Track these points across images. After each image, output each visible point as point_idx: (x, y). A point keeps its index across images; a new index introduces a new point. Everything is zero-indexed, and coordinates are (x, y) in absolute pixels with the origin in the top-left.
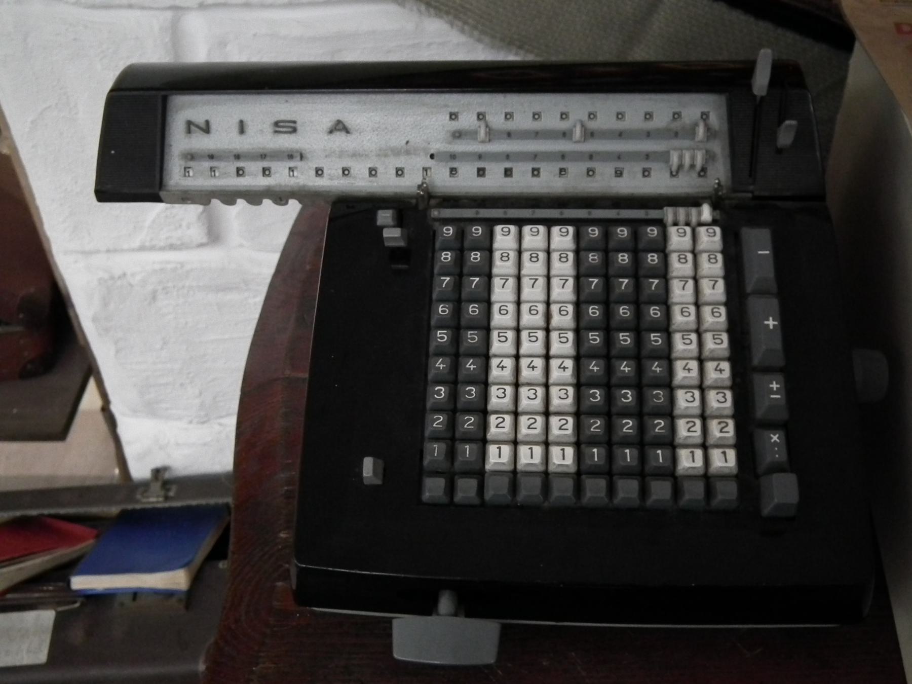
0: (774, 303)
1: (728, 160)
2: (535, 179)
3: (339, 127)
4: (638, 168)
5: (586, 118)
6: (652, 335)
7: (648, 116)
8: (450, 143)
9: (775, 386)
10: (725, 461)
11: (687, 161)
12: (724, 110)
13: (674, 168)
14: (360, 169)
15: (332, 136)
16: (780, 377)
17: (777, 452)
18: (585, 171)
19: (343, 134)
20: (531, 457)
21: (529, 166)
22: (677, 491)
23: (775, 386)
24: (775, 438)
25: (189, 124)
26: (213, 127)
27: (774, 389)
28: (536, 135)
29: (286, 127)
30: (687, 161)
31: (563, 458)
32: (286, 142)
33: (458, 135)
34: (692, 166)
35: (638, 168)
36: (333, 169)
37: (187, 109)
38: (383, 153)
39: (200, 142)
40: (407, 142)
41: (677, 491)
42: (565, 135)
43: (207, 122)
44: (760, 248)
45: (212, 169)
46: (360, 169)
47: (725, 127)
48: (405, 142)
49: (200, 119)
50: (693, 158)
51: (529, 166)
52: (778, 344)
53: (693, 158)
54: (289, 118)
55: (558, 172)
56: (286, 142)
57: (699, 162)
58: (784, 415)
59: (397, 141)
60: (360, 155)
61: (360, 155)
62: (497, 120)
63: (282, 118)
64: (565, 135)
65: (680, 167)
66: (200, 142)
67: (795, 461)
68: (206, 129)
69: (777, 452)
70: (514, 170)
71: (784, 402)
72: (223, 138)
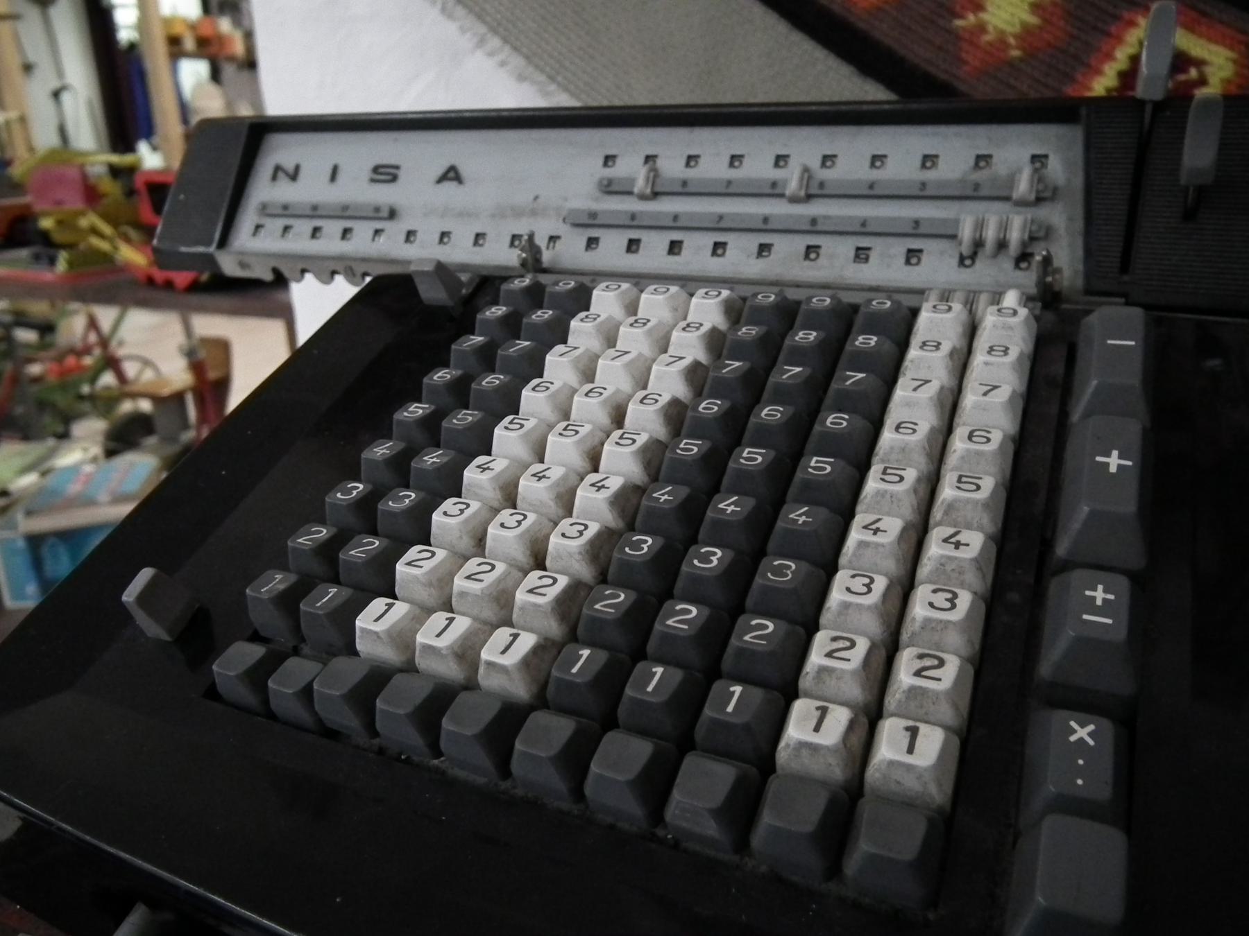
0: (1133, 429)
1: (1079, 242)
2: (716, 259)
3: (452, 175)
4: (899, 248)
5: (815, 163)
6: (815, 459)
7: (929, 160)
8: (596, 200)
9: (1099, 595)
10: (914, 753)
11: (990, 235)
12: (1078, 151)
13: (966, 249)
14: (463, 235)
15: (440, 186)
16: (1123, 582)
17: (1080, 772)
18: (803, 249)
19: (455, 183)
20: (439, 635)
21: (709, 239)
22: (743, 806)
23: (1099, 595)
24: (1082, 732)
25: (278, 169)
26: (303, 174)
27: (1098, 603)
28: (728, 191)
29: (385, 174)
30: (990, 235)
31: (506, 654)
32: (384, 195)
33: (609, 188)
34: (1002, 245)
35: (899, 248)
36: (428, 232)
37: (281, 151)
38: (500, 213)
39: (284, 192)
40: (536, 198)
41: (743, 806)
42: (774, 191)
43: (297, 168)
44: (1116, 339)
45: (286, 229)
46: (463, 235)
47: (1078, 181)
48: (532, 197)
49: (289, 166)
50: (1004, 227)
51: (709, 239)
52: (1127, 503)
53: (1004, 227)
54: (393, 162)
55: (755, 249)
56: (384, 195)
57: (1015, 236)
58: (1120, 682)
59: (522, 198)
60: (469, 215)
61: (469, 215)
62: (672, 167)
63: (385, 162)
64: (774, 191)
65: (978, 244)
66: (284, 192)
67: (1133, 798)
68: (294, 176)
69: (1080, 772)
70: (685, 245)
71: (1121, 634)
72: (311, 189)
